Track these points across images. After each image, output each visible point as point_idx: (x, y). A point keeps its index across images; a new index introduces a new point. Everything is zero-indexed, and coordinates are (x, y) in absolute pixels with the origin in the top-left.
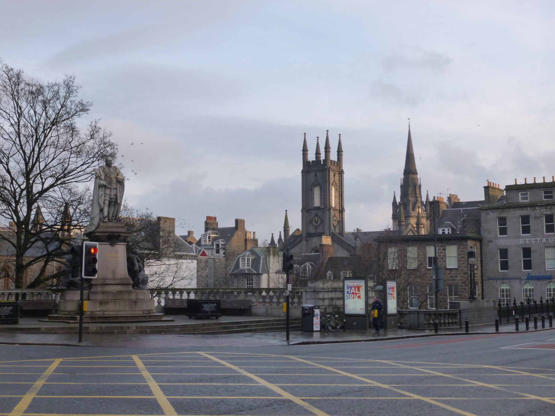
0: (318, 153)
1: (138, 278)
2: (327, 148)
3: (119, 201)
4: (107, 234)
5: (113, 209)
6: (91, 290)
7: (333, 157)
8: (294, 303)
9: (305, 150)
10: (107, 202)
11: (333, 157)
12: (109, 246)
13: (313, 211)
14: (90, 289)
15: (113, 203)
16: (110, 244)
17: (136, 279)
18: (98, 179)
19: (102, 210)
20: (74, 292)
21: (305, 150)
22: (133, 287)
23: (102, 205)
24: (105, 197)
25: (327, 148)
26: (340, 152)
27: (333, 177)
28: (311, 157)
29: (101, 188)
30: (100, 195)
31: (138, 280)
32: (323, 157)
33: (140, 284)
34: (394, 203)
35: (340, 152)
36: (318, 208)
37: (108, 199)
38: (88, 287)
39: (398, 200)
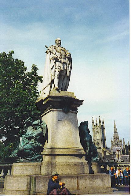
2: (100, 121)
4: (60, 100)
9: (93, 122)
15: (63, 77)
21: (93, 122)
25: (100, 121)
26: (103, 123)
35: (103, 123)
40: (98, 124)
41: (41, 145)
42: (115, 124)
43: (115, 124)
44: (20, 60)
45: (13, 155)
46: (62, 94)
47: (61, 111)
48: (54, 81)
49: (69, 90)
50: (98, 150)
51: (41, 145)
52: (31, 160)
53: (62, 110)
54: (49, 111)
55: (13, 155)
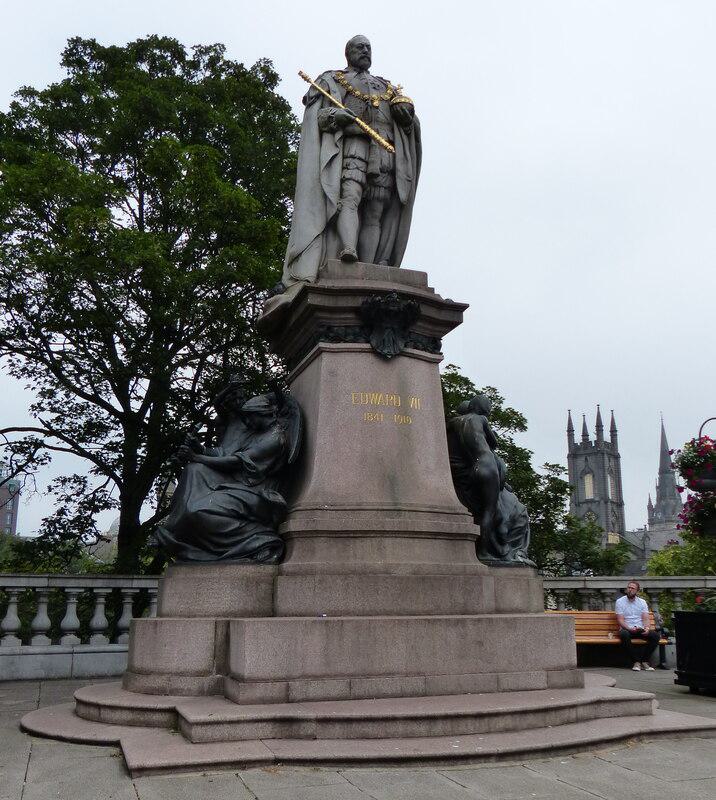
0: (585, 434)
1: (496, 512)
2: (599, 427)
3: (403, 195)
4: (358, 302)
5: (376, 231)
6: (287, 565)
7: (607, 437)
8: (35, 632)
9: (570, 431)
10: (353, 189)
11: (607, 437)
12: (370, 358)
13: (585, 506)
14: (281, 560)
15: (379, 207)
16: (374, 351)
17: (487, 519)
18: (317, 105)
19: (332, 226)
20: (199, 573)
21: (570, 431)
22: (479, 551)
23: (333, 196)
24: (345, 168)
25: (599, 427)
26: (613, 431)
27: (608, 463)
28: (578, 439)
29: (327, 138)
30: (325, 160)
31: (497, 522)
32: (593, 437)
33: (502, 543)
34: (650, 506)
35: (613, 431)
36: (591, 501)
37: (359, 176)
38: (272, 547)
39: (654, 503)
40: (593, 437)
41: (280, 498)
42: (663, 429)
43: (663, 429)
44: (52, 73)
45: (160, 538)
46: (367, 277)
47: (362, 351)
48: (122, 44)
49: (409, 262)
50: (144, 396)
51: (280, 498)
52: (232, 556)
53: (368, 346)
54: (310, 354)
55: (160, 538)
